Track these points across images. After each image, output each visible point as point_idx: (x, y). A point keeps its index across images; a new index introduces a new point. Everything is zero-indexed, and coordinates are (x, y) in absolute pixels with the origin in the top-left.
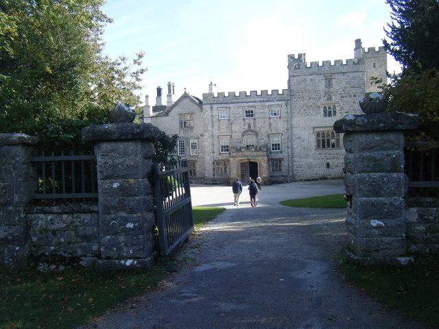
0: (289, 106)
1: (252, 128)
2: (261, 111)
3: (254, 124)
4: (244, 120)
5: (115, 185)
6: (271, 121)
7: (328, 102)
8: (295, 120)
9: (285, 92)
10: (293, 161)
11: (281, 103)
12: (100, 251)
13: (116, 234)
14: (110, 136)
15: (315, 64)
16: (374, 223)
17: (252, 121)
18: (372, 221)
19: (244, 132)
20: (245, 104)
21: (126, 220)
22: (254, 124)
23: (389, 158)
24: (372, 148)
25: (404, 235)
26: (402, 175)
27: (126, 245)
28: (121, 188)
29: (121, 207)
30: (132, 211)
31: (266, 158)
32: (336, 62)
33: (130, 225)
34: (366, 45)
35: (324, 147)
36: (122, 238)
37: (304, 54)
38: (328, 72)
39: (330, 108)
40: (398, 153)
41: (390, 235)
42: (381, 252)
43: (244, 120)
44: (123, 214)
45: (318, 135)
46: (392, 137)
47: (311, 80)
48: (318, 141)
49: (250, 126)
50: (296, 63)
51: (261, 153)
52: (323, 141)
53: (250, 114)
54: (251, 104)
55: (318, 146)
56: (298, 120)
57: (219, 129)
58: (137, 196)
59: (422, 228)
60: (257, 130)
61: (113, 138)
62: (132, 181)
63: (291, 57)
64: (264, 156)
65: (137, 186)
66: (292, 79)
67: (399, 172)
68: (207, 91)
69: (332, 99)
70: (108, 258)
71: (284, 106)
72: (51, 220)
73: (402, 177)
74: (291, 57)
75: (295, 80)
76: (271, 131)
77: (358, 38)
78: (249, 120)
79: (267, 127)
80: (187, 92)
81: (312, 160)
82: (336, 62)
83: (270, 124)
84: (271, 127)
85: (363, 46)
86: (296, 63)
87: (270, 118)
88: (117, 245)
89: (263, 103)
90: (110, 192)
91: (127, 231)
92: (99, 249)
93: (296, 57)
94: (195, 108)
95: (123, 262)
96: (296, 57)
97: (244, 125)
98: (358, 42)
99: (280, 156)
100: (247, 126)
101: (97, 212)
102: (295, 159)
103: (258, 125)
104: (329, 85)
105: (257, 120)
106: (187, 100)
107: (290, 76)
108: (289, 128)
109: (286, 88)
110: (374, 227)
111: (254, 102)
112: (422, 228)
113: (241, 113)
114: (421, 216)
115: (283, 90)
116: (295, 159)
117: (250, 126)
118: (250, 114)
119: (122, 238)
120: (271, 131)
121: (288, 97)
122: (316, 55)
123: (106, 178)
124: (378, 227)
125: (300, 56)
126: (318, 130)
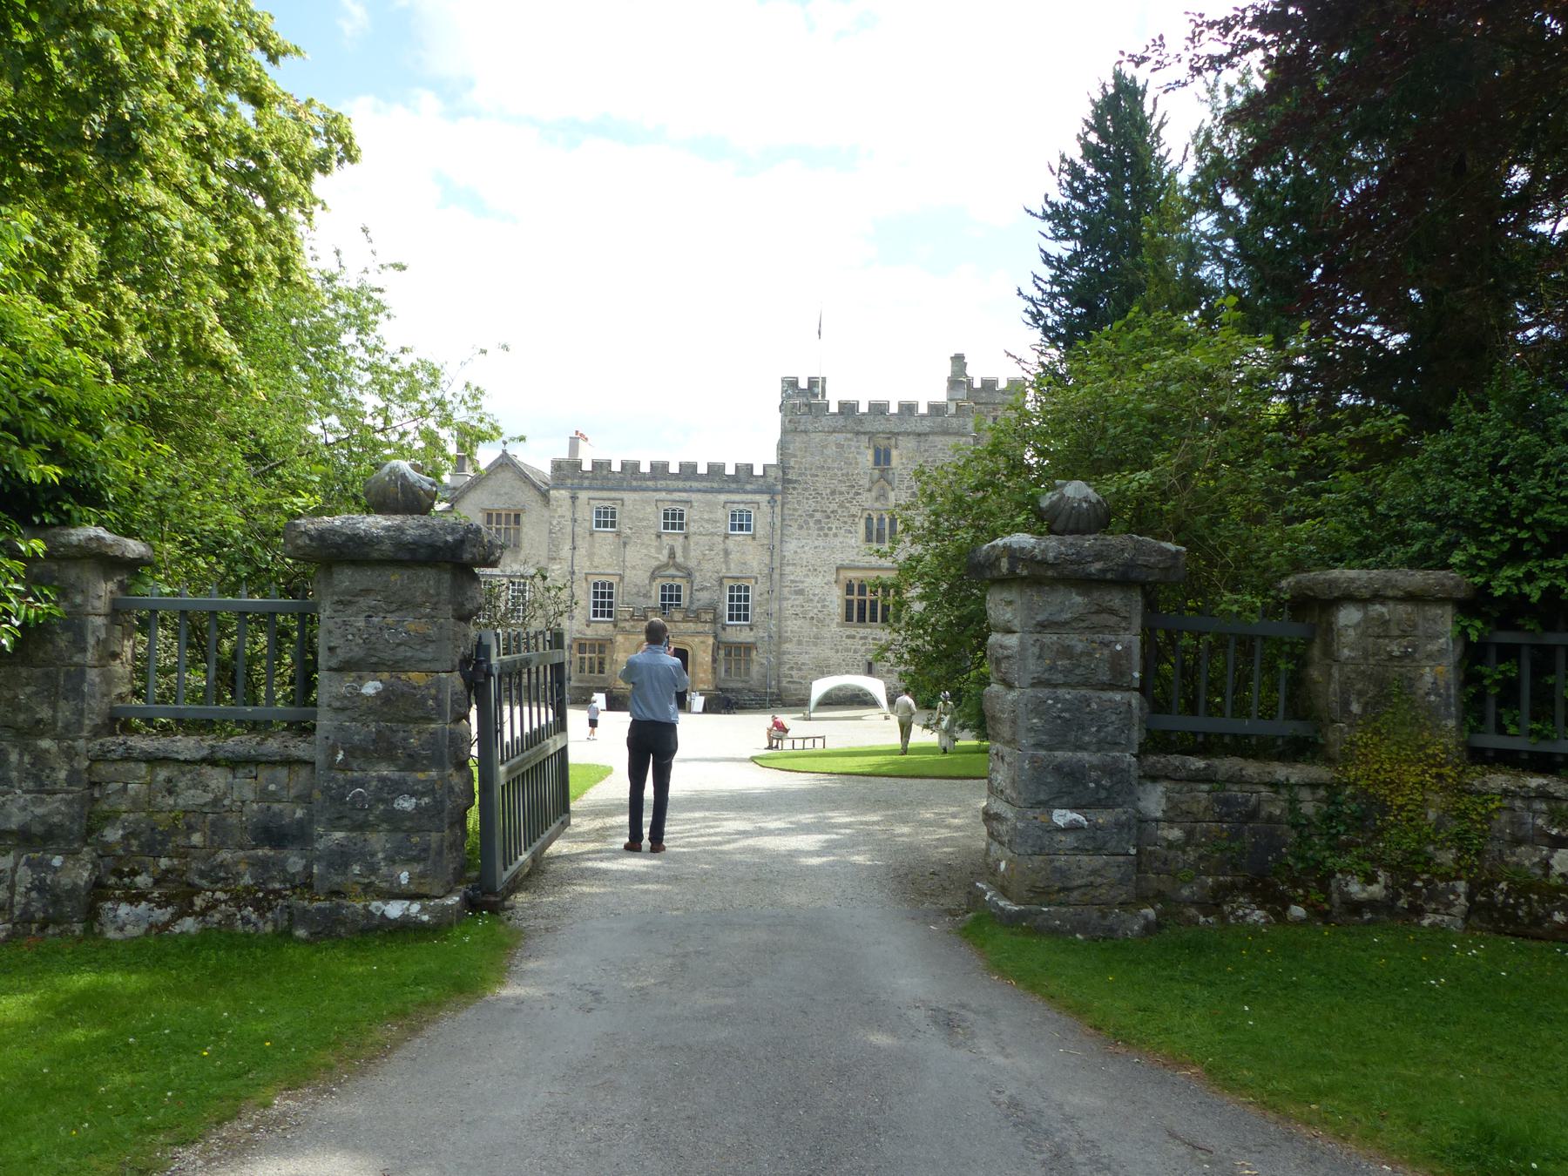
0: (778, 510)
1: (680, 559)
2: (706, 516)
3: (686, 549)
4: (659, 536)
5: (370, 688)
6: (730, 543)
7: (877, 505)
8: (791, 546)
9: (772, 473)
10: (781, 654)
11: (757, 497)
12: (311, 875)
13: (361, 827)
14: (367, 549)
15: (848, 408)
16: (1062, 817)
17: (681, 539)
18: (1057, 812)
19: (658, 568)
20: (663, 495)
21: (398, 788)
22: (686, 549)
23: (1106, 652)
24: (1065, 623)
25: (1133, 851)
26: (1135, 699)
27: (391, 860)
28: (386, 697)
29: (383, 748)
30: (413, 762)
31: (711, 641)
32: (872, 406)
33: (406, 804)
34: (977, 373)
35: (861, 619)
36: (378, 841)
37: (824, 379)
38: (876, 428)
39: (881, 520)
40: (1129, 641)
41: (1097, 851)
42: (1075, 894)
43: (659, 536)
44: (386, 771)
45: (849, 589)
46: (1115, 599)
47: (839, 446)
48: (849, 604)
49: (672, 555)
50: (802, 403)
51: (700, 628)
52: (862, 605)
53: (674, 520)
54: (676, 496)
55: (849, 618)
56: (801, 548)
57: (591, 555)
58: (430, 720)
59: (1175, 834)
60: (692, 564)
61: (376, 555)
62: (416, 677)
63: (791, 384)
64: (704, 633)
65: (433, 691)
66: (789, 437)
67: (1129, 689)
68: (563, 454)
69: (887, 499)
70: (335, 893)
71: (765, 507)
72: (169, 780)
73: (1134, 702)
74: (791, 384)
75: (798, 442)
76: (728, 569)
77: (959, 352)
78: (674, 539)
79: (720, 558)
80: (510, 452)
81: (829, 653)
82: (872, 406)
83: (727, 553)
84: (717, 553)
85: (969, 372)
86: (802, 403)
87: (727, 536)
88: (365, 856)
89: (710, 496)
90: (351, 705)
91: (394, 820)
92: (308, 867)
93: (803, 384)
94: (527, 497)
95: (375, 905)
96: (803, 384)
97: (659, 549)
98: (958, 360)
99: (745, 636)
100: (666, 552)
101: (310, 764)
102: (787, 646)
103: (694, 553)
104: (882, 457)
105: (692, 540)
106: (507, 476)
107: (784, 432)
108: (776, 564)
109: (773, 461)
110: (1059, 829)
111: (685, 491)
112: (1175, 834)
113: (652, 517)
114: (1173, 805)
115: (765, 467)
116: (787, 646)
117: (672, 555)
118: (674, 520)
119: (378, 841)
120: (728, 569)
121: (779, 483)
122: (851, 384)
123: (343, 668)
124: (1073, 828)
125: (812, 382)
126: (851, 574)
